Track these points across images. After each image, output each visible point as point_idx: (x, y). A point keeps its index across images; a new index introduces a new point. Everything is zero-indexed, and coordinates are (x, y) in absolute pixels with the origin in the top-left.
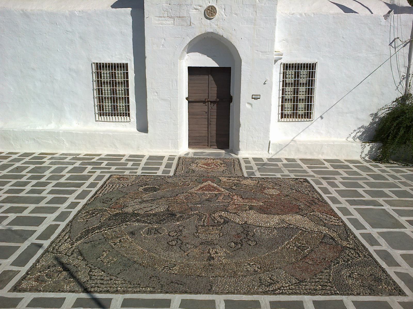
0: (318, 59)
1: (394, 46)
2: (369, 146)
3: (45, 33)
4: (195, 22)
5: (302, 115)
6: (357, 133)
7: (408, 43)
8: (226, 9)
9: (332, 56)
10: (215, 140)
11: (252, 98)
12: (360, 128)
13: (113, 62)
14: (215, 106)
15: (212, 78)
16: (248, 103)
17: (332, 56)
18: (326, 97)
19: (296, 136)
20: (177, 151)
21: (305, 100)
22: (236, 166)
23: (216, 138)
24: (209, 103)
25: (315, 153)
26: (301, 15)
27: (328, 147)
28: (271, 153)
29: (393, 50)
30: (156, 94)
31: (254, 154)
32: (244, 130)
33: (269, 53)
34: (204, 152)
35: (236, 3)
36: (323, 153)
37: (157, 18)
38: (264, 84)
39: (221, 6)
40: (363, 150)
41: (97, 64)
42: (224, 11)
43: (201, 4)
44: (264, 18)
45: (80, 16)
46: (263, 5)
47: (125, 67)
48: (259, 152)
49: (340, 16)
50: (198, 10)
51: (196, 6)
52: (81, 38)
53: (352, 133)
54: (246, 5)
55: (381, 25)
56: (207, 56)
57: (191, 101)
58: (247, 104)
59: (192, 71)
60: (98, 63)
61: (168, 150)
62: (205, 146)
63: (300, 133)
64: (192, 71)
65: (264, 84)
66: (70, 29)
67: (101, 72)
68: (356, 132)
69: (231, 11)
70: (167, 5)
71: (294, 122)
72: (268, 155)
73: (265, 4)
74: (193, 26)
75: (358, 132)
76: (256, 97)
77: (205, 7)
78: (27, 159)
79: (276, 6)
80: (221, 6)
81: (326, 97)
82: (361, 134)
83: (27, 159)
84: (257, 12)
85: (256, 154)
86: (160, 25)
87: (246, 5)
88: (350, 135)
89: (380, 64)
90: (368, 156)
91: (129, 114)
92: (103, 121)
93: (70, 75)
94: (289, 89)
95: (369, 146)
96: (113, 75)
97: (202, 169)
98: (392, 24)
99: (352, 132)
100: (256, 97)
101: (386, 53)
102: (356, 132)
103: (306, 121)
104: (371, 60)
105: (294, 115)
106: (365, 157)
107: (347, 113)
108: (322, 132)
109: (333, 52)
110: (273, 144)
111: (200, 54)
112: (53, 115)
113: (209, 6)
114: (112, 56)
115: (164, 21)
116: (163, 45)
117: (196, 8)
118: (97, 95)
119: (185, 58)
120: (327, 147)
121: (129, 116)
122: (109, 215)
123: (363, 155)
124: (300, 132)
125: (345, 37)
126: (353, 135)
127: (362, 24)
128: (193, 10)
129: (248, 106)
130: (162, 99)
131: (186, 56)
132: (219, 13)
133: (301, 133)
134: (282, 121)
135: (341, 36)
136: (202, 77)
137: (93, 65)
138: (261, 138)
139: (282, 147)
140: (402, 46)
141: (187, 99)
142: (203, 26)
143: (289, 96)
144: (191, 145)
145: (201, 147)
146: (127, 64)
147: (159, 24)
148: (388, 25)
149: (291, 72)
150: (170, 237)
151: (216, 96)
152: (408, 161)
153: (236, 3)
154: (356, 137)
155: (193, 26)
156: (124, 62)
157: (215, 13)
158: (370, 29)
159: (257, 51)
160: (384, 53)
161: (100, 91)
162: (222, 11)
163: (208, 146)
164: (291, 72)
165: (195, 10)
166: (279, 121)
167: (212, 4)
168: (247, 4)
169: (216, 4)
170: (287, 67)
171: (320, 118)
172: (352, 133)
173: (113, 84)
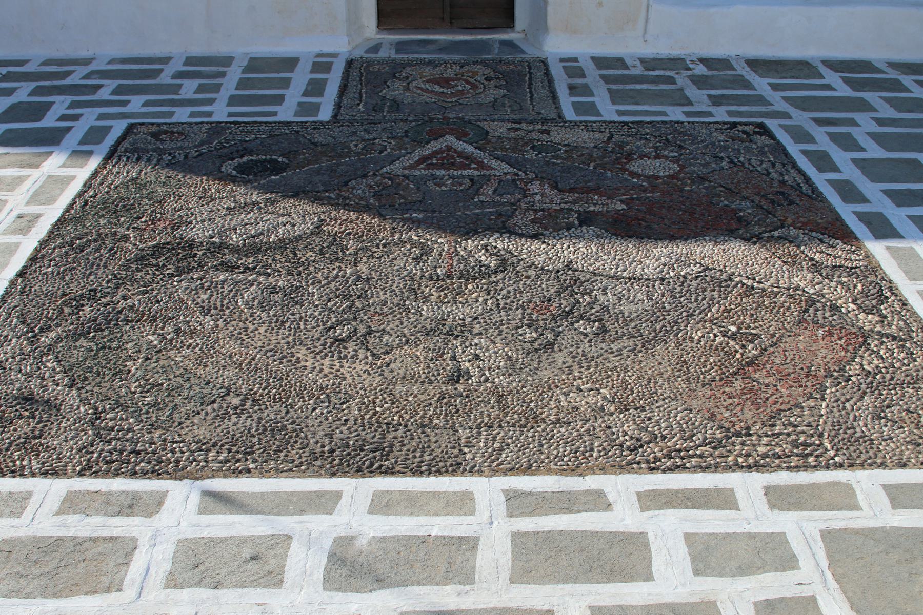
22: (537, 84)
97: (426, 97)
163: (443, 19)
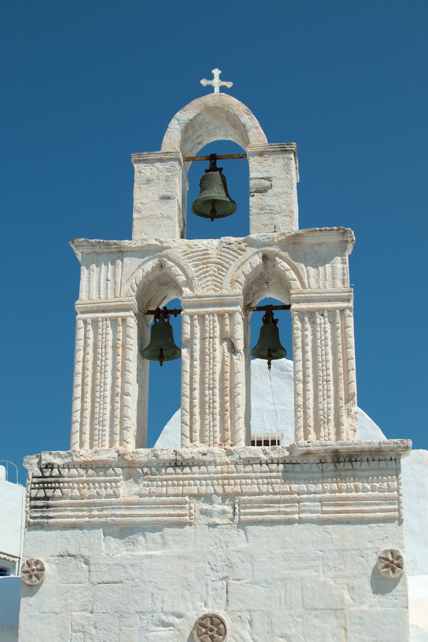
8: (254, 623)
35: (283, 606)
39: (240, 614)
42: (249, 628)
43: (181, 610)
46: (365, 607)
50: (171, 628)
69: (272, 627)
70: (84, 613)
77: (194, 616)
79: (405, 610)
80: (240, 614)
84: (348, 628)
87: (315, 609)
112: (202, 197)
113: (205, 617)
117: (166, 621)
122: (71, 461)
128: (158, 626)
132: (236, 636)
141: (212, 220)
150: (114, 548)
152: (427, 448)
153: (283, 606)
157: (221, 635)
162: (245, 628)
165: (162, 628)
167: (213, 609)
168: (317, 606)
169: (226, 610)
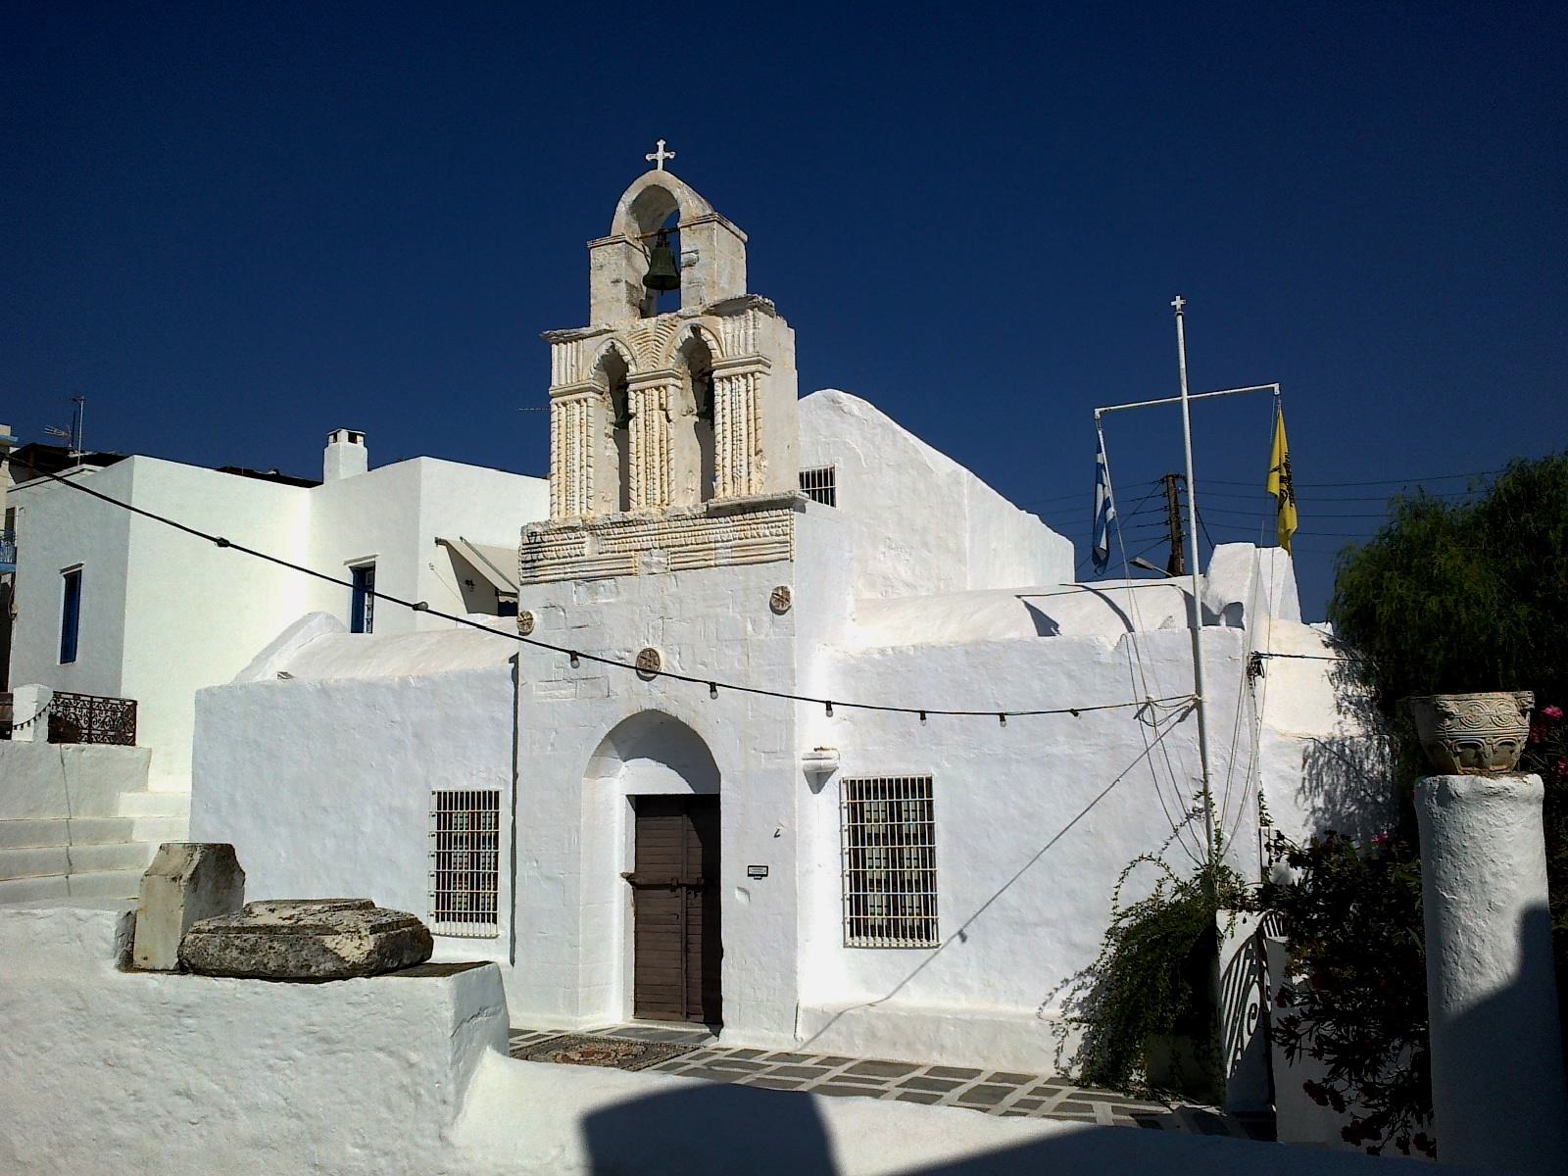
0: (938, 766)
1: (1151, 721)
2: (1077, 1029)
3: (354, 729)
4: (619, 689)
5: (881, 927)
6: (1075, 990)
7: (1192, 709)
9: (972, 756)
10: (698, 998)
11: (749, 875)
12: (1081, 974)
13: (476, 789)
14: (699, 897)
15: (691, 823)
16: (739, 888)
17: (972, 756)
18: (969, 874)
19: (895, 992)
20: (573, 1018)
21: (887, 882)
23: (703, 992)
24: (684, 889)
25: (919, 1046)
26: (882, 652)
27: (955, 1027)
28: (802, 1039)
29: (1149, 731)
30: (535, 865)
31: (758, 1040)
32: (733, 968)
33: (782, 756)
34: (692, 1033)
36: (942, 1048)
37: (543, 684)
38: (776, 836)
40: (1060, 1045)
41: (853, 782)
43: (630, 646)
44: (767, 668)
45: (419, 688)
46: (762, 637)
47: (493, 798)
48: (772, 1035)
49: (983, 648)
51: (619, 651)
52: (416, 735)
53: (1057, 989)
54: (726, 641)
55: (1100, 663)
56: (668, 766)
57: (639, 884)
58: (737, 892)
59: (644, 806)
60: (855, 781)
61: (553, 1016)
62: (672, 1015)
63: (904, 983)
64: (644, 806)
65: (776, 836)
66: (397, 718)
67: (899, 804)
68: (1072, 985)
71: (886, 948)
72: (794, 1043)
73: (767, 636)
74: (613, 698)
75: (1079, 988)
76: (758, 873)
78: (838, 1071)
81: (969, 874)
82: (1087, 993)
83: (838, 1071)
85: (763, 1039)
86: (549, 700)
87: (726, 641)
88: (1050, 994)
89: (1117, 773)
90: (1080, 1067)
91: (495, 915)
92: (910, 948)
93: (389, 820)
94: (874, 851)
95: (1077, 1029)
96: (894, 812)
98: (1134, 659)
99: (1059, 986)
100: (758, 873)
101: (1130, 742)
102: (1072, 985)
103: (918, 948)
104: (1086, 765)
105: (895, 930)
106: (1070, 1068)
107: (1036, 925)
108: (969, 982)
109: (975, 746)
110: (806, 1011)
111: (653, 763)
114: (472, 775)
115: (557, 690)
116: (552, 745)
118: (850, 867)
119: (620, 774)
120: (952, 1029)
121: (495, 922)
123: (1064, 1063)
124: (904, 979)
125: (1001, 703)
126: (1063, 995)
127: (1046, 664)
129: (739, 896)
130: (548, 878)
131: (623, 767)
133: (908, 983)
134: (885, 945)
135: (992, 701)
136: (666, 821)
137: (844, 786)
138: (774, 989)
139: (831, 1019)
140: (1175, 718)
141: (629, 877)
142: (633, 696)
143: (876, 871)
144: (642, 1009)
145: (664, 1015)
146: (929, 781)
147: (546, 697)
148: (1123, 662)
149: (874, 805)
151: (700, 870)
154: (1071, 1005)
155: (613, 698)
156: (493, 788)
158: (1071, 677)
159: (755, 749)
160: (1123, 742)
161: (857, 858)
164: (874, 805)
166: (845, 945)
170: (859, 790)
171: (958, 937)
172: (1057, 989)
173: (895, 835)
